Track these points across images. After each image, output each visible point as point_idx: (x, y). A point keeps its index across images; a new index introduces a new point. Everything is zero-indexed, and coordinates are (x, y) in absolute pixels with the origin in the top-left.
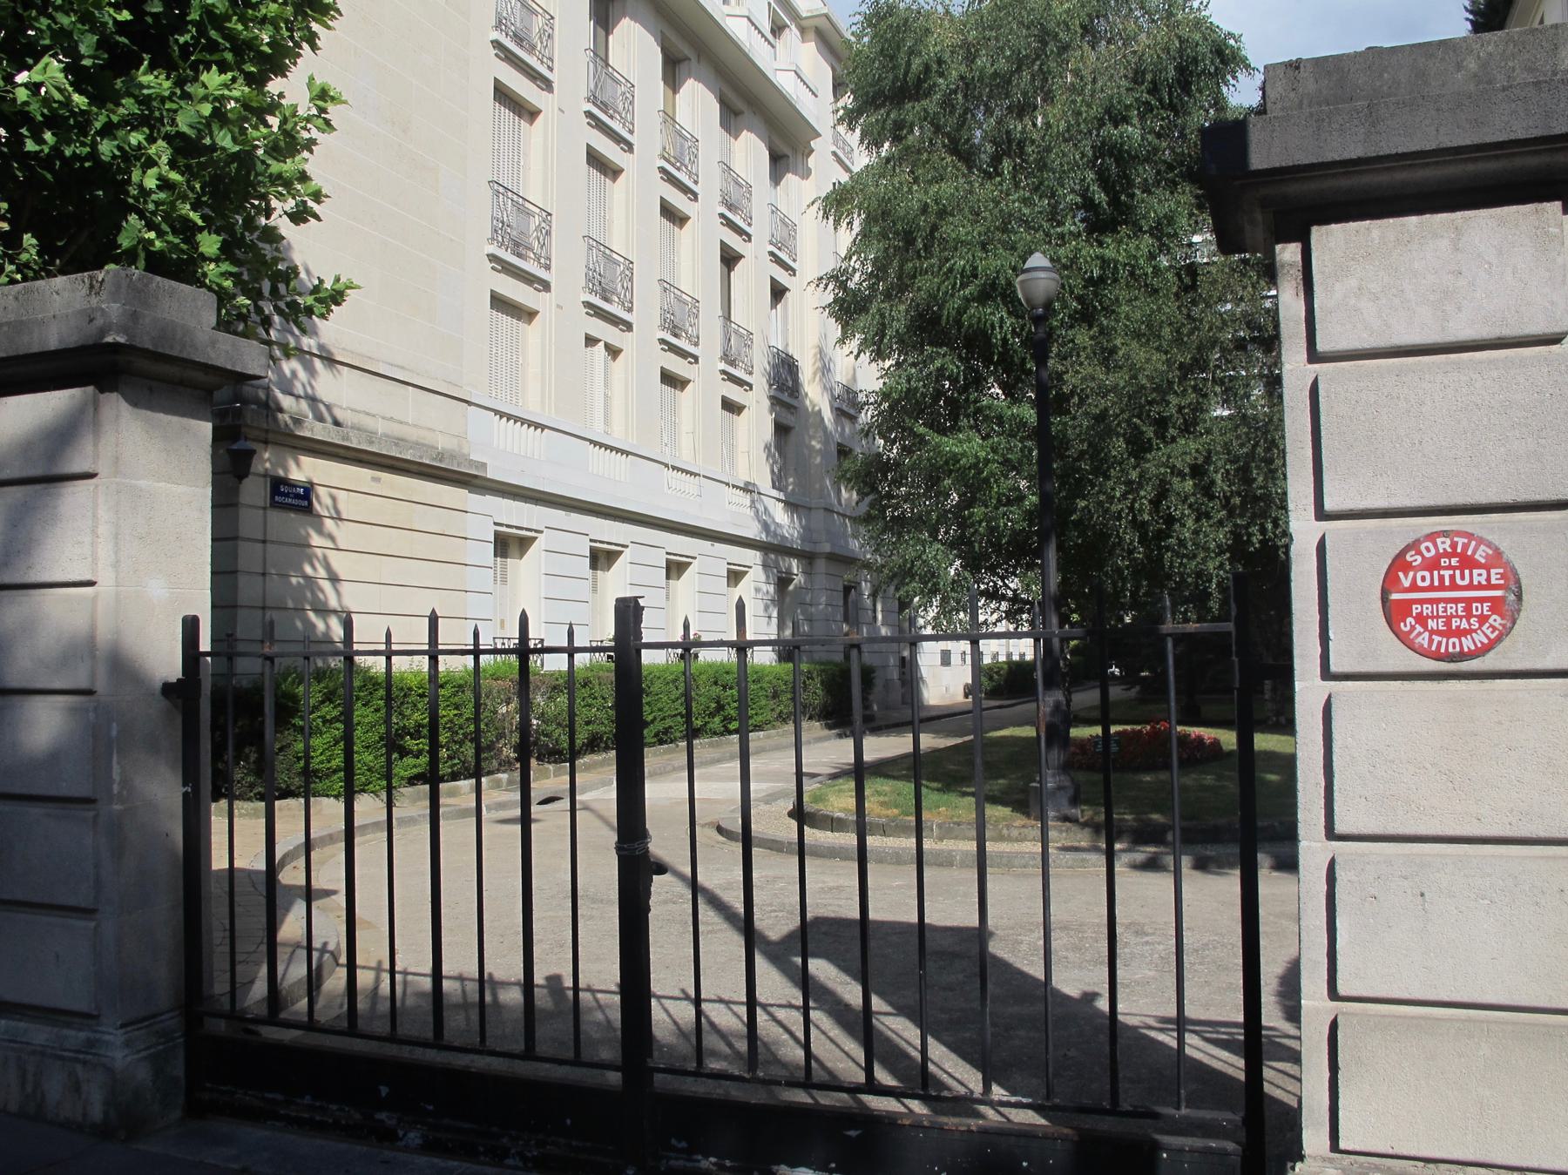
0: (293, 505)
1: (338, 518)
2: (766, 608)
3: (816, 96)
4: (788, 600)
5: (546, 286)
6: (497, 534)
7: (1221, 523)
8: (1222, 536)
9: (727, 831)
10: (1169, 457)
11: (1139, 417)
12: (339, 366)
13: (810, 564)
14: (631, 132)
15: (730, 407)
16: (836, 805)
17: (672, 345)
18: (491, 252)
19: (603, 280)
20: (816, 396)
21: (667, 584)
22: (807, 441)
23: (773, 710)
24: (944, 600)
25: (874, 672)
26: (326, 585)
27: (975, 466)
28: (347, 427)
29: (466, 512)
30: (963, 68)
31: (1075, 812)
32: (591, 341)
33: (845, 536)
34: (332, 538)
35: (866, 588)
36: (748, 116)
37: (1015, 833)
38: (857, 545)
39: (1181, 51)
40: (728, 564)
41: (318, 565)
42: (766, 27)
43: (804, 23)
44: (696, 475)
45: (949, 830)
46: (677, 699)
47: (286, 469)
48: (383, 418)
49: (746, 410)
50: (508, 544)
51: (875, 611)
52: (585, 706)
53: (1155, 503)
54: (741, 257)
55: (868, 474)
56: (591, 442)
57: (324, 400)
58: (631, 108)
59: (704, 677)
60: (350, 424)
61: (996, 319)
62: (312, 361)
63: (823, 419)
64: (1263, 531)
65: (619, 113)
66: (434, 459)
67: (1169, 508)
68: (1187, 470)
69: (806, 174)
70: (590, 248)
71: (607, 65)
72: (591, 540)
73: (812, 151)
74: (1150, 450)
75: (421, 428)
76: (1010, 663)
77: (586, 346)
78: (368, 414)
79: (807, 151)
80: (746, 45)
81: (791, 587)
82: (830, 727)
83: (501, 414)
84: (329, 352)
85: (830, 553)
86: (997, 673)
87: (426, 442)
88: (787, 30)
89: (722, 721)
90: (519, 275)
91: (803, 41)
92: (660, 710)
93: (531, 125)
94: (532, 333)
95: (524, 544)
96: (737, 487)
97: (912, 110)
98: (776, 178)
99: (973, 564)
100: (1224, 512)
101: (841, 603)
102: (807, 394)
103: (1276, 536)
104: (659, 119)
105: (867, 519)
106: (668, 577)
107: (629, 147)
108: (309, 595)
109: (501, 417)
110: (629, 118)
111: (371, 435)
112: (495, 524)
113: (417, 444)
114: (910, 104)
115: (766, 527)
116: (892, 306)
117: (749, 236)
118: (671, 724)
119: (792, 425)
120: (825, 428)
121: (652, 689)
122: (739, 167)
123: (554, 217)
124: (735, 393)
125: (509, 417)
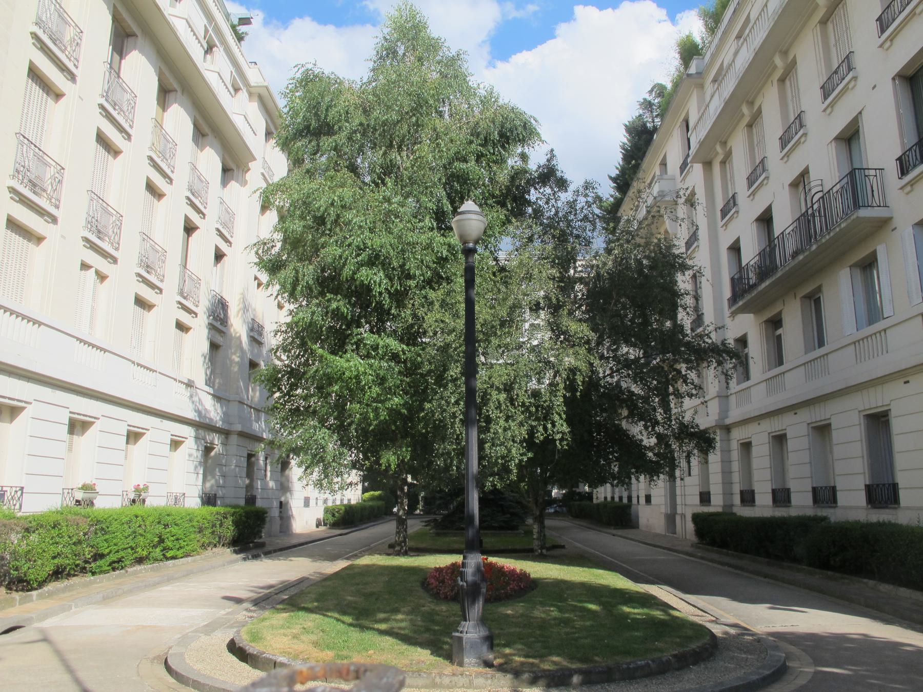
2: (196, 467)
4: (210, 461)
5: (54, 220)
7: (521, 424)
8: (524, 432)
9: (176, 673)
15: (181, 327)
17: (146, 279)
18: (11, 185)
20: (238, 327)
21: (127, 448)
23: (198, 541)
25: (266, 513)
32: (85, 266)
33: (250, 421)
36: (210, 138)
37: (446, 680)
40: (129, 425)
43: (252, 90)
46: (129, 536)
49: (192, 330)
50: (77, 426)
51: (266, 471)
52: (53, 543)
54: (197, 228)
56: (78, 339)
58: (133, 111)
59: (151, 519)
61: (378, 280)
63: (241, 342)
64: (545, 429)
65: (124, 112)
67: (488, 411)
68: (501, 387)
69: (244, 183)
71: (119, 77)
73: (249, 170)
76: (345, 506)
77: (81, 270)
79: (246, 169)
81: (213, 454)
82: (236, 552)
85: (240, 432)
89: (162, 551)
90: (31, 206)
92: (115, 545)
93: (56, 103)
94: (37, 252)
98: (225, 182)
101: (245, 465)
102: (232, 325)
103: (553, 432)
104: (151, 124)
106: (127, 443)
107: (129, 137)
110: (131, 117)
115: (199, 412)
116: (304, 266)
121: (110, 529)
122: (201, 167)
123: (66, 171)
124: (186, 318)
125: (12, 312)
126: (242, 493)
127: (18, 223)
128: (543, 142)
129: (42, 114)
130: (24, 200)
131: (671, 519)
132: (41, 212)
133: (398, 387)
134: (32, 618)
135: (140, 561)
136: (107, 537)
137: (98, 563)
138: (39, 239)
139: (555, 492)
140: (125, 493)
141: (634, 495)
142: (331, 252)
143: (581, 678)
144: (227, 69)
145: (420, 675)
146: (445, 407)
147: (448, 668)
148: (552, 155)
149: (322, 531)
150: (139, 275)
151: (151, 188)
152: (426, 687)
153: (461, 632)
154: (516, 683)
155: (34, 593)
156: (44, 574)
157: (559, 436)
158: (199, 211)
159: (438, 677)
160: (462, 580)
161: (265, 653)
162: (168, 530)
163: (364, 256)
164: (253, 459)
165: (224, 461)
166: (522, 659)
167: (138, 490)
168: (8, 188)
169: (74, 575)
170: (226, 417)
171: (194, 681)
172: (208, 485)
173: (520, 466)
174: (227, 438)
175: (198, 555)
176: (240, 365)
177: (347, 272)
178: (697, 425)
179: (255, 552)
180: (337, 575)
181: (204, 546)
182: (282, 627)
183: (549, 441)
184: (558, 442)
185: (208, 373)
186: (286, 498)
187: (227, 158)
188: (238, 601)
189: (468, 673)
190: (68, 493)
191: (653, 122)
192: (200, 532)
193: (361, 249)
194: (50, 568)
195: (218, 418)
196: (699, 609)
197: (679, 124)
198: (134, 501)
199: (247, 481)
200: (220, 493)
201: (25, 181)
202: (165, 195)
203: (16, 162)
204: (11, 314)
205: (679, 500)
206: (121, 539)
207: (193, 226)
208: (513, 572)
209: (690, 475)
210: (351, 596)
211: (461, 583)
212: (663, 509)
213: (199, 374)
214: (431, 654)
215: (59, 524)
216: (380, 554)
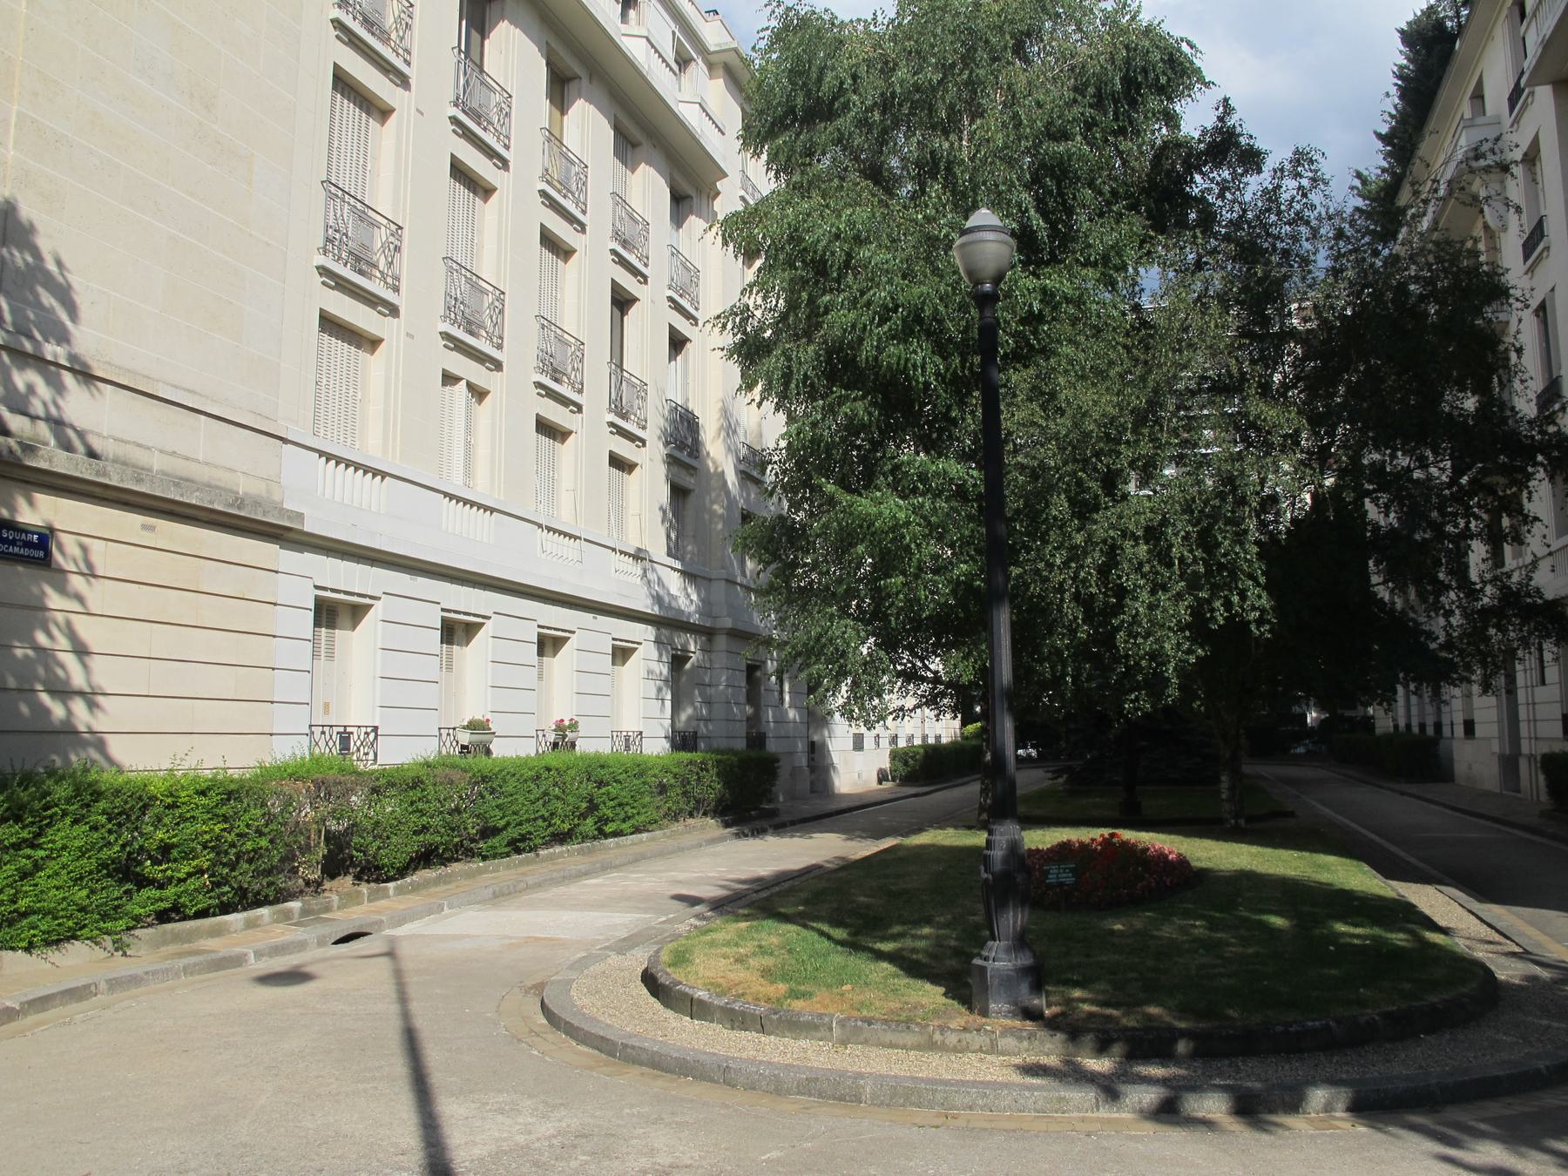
0: (22, 556)
1: (90, 573)
2: (659, 690)
3: (723, 134)
4: (684, 679)
5: (394, 311)
6: (444, 620)
7: (1179, 596)
8: (1183, 612)
10: (1120, 517)
11: (1083, 470)
12: (100, 384)
13: (710, 640)
14: (507, 147)
15: (619, 464)
16: (701, 971)
19: (467, 311)
20: (719, 455)
21: (541, 664)
22: (708, 505)
24: (855, 684)
25: (778, 761)
26: (69, 660)
27: (894, 529)
28: (107, 460)
29: (276, 572)
30: (880, 83)
31: (1038, 1002)
32: (449, 379)
34: (79, 598)
35: (771, 666)
36: (646, 147)
37: (952, 1039)
38: (766, 621)
39: (1128, 61)
41: (55, 632)
42: (670, 56)
43: (712, 58)
44: (576, 538)
45: (857, 1030)
46: (538, 799)
47: (13, 509)
48: (161, 451)
49: (638, 468)
50: (455, 631)
51: (781, 692)
53: (1104, 571)
55: (771, 539)
56: (446, 494)
57: (76, 424)
59: (572, 772)
60: (111, 456)
61: (919, 360)
62: (59, 375)
63: (725, 482)
64: (1228, 604)
66: (231, 505)
67: (1120, 577)
70: (451, 270)
71: (482, 71)
72: (443, 610)
73: (718, 193)
74: (1096, 509)
75: (216, 467)
76: (925, 746)
78: (139, 445)
80: (645, 69)
81: (688, 666)
82: (727, 825)
83: (329, 457)
84: (85, 364)
86: (912, 758)
87: (222, 485)
88: (693, 63)
89: (596, 823)
90: (345, 287)
91: (711, 78)
92: (515, 813)
94: (374, 364)
95: (356, 612)
96: (626, 554)
97: (824, 132)
98: (678, 219)
99: (889, 643)
100: (1183, 584)
102: (708, 454)
103: (1243, 610)
104: (539, 138)
105: (771, 589)
107: (504, 164)
108: (41, 671)
109: (328, 460)
111: (140, 472)
112: (317, 587)
113: (209, 486)
114: (823, 125)
115: (658, 599)
116: (798, 346)
117: (645, 278)
118: (529, 829)
119: (691, 487)
120: (728, 493)
122: (636, 201)
124: (625, 449)
125: (339, 461)
126: (742, 730)
127: (339, 322)
128: (1207, 85)
129: (362, 146)
130: (342, 285)
131: (1509, 763)
132: (371, 300)
133: (968, 544)
134: (382, 921)
135: (561, 838)
136: (500, 801)
137: (490, 843)
138: (373, 343)
139: (1312, 716)
140: (540, 734)
141: (1445, 720)
142: (840, 319)
143: (1191, 1045)
144: (664, 31)
145: (908, 1028)
146: (1045, 573)
147: (960, 1016)
148: (1226, 107)
149: (884, 790)
150: (539, 385)
151: (549, 241)
152: (918, 1047)
153: (986, 959)
154: (1071, 1049)
155: (391, 885)
156: (402, 859)
157: (1255, 615)
158: (635, 272)
159: (938, 1032)
160: (986, 871)
161: (680, 983)
162: (603, 790)
163: (896, 320)
164: (758, 674)
165: (707, 680)
166: (1094, 1009)
167: (560, 727)
168: (317, 268)
169: (457, 860)
170: (707, 607)
171: (567, 1023)
172: (683, 717)
173: (1180, 671)
174: (710, 640)
175: (661, 829)
176: (726, 520)
177: (867, 350)
178: (1538, 590)
179: (758, 824)
180: (866, 859)
181: (674, 816)
182: (728, 944)
183: (1237, 626)
184: (1253, 627)
185: (673, 536)
186: (823, 736)
187: (679, 178)
188: (693, 901)
189: (988, 1028)
190: (323, 733)
191: (1458, 15)
192: (661, 793)
193: (888, 310)
194: (414, 846)
195: (693, 608)
196: (1497, 931)
197: (1505, 12)
198: (555, 745)
199: (749, 710)
200: (703, 730)
201: (344, 255)
202: (574, 251)
203: (327, 227)
204: (337, 464)
205: (1524, 728)
206: (523, 805)
207: (629, 298)
208: (1162, 857)
209: (1543, 683)
210: (866, 896)
211: (985, 876)
212: (1496, 748)
213: (656, 542)
214: (945, 995)
215: (422, 782)
216: (956, 827)
